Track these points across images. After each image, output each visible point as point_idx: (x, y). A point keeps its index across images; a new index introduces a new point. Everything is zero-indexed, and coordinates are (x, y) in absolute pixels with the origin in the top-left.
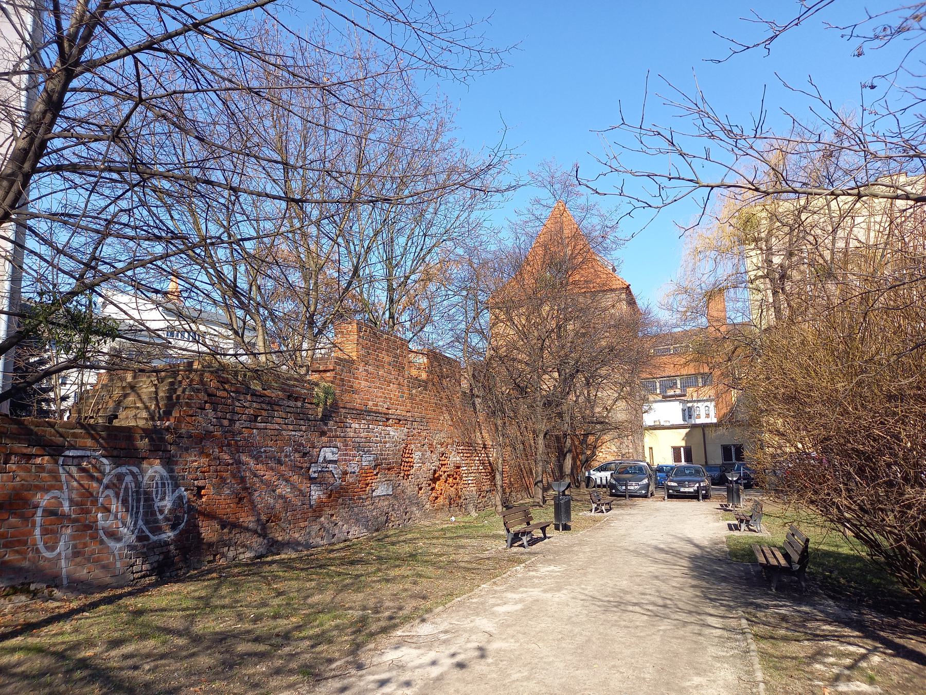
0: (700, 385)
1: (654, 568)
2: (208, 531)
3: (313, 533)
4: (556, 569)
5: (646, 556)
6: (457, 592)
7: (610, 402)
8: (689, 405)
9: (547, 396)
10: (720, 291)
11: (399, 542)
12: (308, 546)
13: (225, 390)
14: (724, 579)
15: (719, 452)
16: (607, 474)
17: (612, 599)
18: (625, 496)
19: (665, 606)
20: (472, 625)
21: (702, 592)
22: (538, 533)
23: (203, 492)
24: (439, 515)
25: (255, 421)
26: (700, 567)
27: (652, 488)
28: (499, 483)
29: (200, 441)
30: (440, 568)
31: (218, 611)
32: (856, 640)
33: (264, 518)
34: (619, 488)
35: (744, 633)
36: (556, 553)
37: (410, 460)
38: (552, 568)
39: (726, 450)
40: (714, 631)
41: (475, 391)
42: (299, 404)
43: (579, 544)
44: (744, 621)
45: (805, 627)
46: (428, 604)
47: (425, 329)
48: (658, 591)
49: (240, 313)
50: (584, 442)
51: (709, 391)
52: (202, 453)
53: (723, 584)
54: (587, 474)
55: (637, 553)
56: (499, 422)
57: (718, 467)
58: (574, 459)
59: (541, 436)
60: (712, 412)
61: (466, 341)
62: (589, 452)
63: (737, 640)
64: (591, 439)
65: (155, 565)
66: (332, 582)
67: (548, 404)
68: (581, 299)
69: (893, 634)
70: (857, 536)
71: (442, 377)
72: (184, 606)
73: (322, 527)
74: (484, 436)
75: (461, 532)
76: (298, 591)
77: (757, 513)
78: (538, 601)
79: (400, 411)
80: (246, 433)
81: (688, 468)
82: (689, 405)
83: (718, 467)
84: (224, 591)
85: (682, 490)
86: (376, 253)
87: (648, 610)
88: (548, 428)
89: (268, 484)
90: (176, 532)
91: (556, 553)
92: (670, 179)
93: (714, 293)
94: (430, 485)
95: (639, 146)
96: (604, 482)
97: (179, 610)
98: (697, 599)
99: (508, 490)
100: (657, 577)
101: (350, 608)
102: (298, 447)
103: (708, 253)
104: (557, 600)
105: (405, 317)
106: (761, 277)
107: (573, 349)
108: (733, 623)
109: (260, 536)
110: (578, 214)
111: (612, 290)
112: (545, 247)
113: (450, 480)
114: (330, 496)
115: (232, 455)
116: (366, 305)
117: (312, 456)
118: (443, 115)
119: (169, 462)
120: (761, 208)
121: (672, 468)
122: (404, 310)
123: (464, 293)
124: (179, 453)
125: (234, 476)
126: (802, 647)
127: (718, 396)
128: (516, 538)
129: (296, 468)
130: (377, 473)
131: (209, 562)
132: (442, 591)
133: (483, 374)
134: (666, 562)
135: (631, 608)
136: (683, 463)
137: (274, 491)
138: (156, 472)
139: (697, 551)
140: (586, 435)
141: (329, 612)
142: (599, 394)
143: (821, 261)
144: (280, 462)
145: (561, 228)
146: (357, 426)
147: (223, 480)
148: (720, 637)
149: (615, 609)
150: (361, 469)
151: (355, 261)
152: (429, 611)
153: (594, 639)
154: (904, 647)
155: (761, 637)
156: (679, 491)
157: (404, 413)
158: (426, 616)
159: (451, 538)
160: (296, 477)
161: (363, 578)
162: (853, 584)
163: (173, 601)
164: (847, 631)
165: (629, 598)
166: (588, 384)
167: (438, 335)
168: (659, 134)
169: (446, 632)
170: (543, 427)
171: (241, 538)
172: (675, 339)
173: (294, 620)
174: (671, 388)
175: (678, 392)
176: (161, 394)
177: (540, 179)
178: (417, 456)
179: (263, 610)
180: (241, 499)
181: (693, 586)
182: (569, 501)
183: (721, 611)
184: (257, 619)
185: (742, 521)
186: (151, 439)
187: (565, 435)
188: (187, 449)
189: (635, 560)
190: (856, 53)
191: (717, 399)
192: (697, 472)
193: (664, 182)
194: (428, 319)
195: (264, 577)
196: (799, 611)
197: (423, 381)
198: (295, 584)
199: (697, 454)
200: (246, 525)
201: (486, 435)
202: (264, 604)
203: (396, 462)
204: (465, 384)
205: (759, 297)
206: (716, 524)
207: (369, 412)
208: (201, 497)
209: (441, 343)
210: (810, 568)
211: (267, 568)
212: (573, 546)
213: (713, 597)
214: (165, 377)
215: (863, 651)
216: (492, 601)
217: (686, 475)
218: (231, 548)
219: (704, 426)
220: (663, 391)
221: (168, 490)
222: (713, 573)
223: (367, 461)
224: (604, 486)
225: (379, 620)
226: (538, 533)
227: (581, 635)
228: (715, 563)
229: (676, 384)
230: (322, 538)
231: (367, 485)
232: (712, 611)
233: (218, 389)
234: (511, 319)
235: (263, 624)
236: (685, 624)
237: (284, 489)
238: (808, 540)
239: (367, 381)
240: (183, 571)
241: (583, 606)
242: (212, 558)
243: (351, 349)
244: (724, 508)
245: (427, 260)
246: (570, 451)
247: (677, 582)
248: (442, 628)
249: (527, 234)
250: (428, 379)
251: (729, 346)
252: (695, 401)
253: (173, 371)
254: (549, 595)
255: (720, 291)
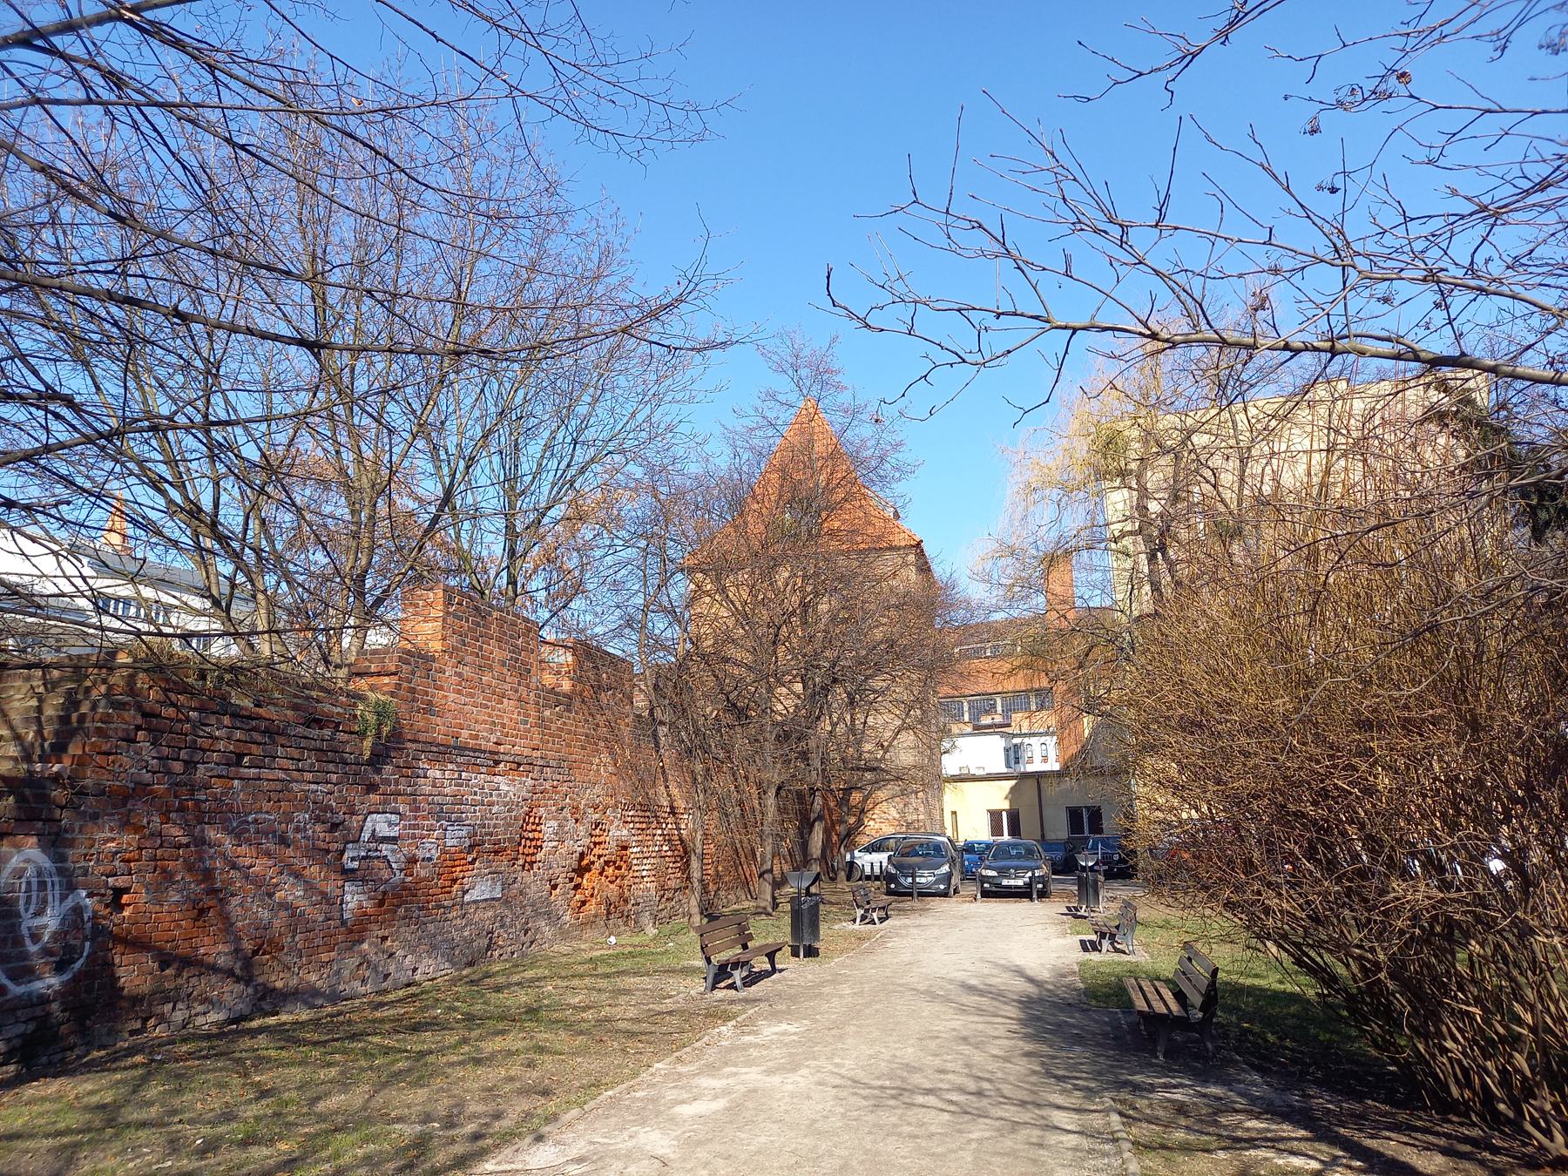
0: (1033, 708)
1: (959, 1023)
2: (133, 974)
3: (346, 973)
4: (791, 1029)
5: (947, 1000)
6: (608, 1079)
7: (888, 734)
8: (1017, 741)
9: (782, 724)
10: (1068, 553)
11: (509, 985)
12: (335, 997)
13: (173, 705)
14: (1078, 1040)
15: (1063, 818)
16: (881, 858)
17: (887, 1083)
18: (910, 895)
19: (979, 1093)
20: (630, 1144)
21: (1043, 1064)
22: (761, 964)
23: (125, 898)
24: (588, 934)
25: (239, 764)
26: (1039, 1019)
27: (955, 880)
28: (696, 875)
29: (122, 802)
30: (581, 1033)
31: (130, 1134)
32: (1303, 1146)
33: (247, 946)
34: (902, 880)
35: (1117, 1140)
36: (793, 999)
37: (536, 835)
38: (784, 1027)
39: (1074, 815)
40: (1065, 1138)
41: (658, 713)
42: (327, 732)
43: (833, 982)
44: (1115, 1118)
45: (1216, 1123)
46: (552, 1106)
47: (572, 605)
48: (967, 1065)
49: (226, 568)
50: (844, 801)
51: (1048, 719)
52: (126, 824)
53: (1078, 1049)
54: (848, 857)
55: (932, 996)
56: (699, 767)
57: (1064, 843)
58: (827, 832)
59: (772, 793)
60: (1052, 753)
61: (644, 627)
62: (852, 820)
63: (1105, 1154)
64: (856, 797)
65: (17, 1042)
66: (371, 1068)
67: (784, 737)
68: (841, 561)
69: (1360, 1130)
70: (1299, 962)
71: (598, 688)
72: (61, 1126)
73: (365, 961)
74: (673, 792)
75: (626, 965)
76: (299, 1088)
77: (1129, 920)
78: (755, 1091)
79: (521, 749)
80: (218, 787)
81: (1014, 846)
82: (1017, 741)
83: (1064, 843)
84: (153, 1090)
85: (1005, 882)
86: (487, 471)
87: (951, 1102)
88: (784, 777)
89: (259, 882)
90: (66, 977)
91: (793, 999)
92: (998, 315)
93: (1053, 560)
94: (571, 880)
95: (945, 242)
96: (877, 870)
97: (47, 1136)
98: (1034, 1079)
99: (712, 887)
100: (965, 1039)
101: (399, 1120)
102: (321, 813)
103: (1047, 492)
104: (790, 1087)
105: (537, 583)
106: (1131, 533)
107: (828, 642)
108: (1097, 1121)
109: (238, 980)
110: (839, 419)
111: (891, 548)
112: (783, 471)
113: (610, 871)
114: (381, 903)
115: (187, 827)
116: (464, 557)
117: (349, 829)
118: (611, 237)
119: (55, 842)
120: (1129, 423)
121: (989, 846)
122: (535, 571)
123: (642, 544)
124: (77, 825)
125: (190, 868)
126: (1216, 1162)
127: (1062, 726)
128: (722, 972)
129: (317, 852)
130: (474, 860)
131: (133, 1033)
132: (579, 1078)
133: (673, 685)
134: (980, 1011)
135: (920, 1099)
136: (1006, 837)
137: (271, 895)
138: (28, 861)
139: (1031, 989)
140: (848, 791)
141: (355, 1130)
142: (870, 720)
143: (1222, 509)
144: (283, 841)
145: (811, 441)
146: (438, 774)
147: (168, 876)
148: (1075, 1149)
149: (892, 1102)
150: (444, 852)
151: (447, 480)
152: (552, 1118)
153: (854, 1163)
154: (1380, 1155)
155: (1146, 1147)
156: (999, 885)
157: (527, 752)
158: (545, 1129)
159: (607, 976)
160: (315, 869)
161: (431, 1059)
162: (1288, 1043)
163: (41, 1115)
164: (1286, 1130)
165: (917, 1079)
166: (852, 702)
167: (594, 614)
168: (980, 226)
169: (580, 1160)
170: (775, 776)
171: (200, 985)
172: (996, 631)
173: (283, 1146)
174: (987, 712)
175: (998, 719)
176: (49, 712)
177: (775, 358)
178: (549, 827)
179: (222, 1129)
180: (202, 912)
181: (1028, 1054)
182: (817, 905)
183: (1075, 1099)
184: (211, 1146)
185: (1103, 936)
186: (21, 799)
187: (813, 791)
188: (95, 817)
189: (928, 1009)
190: (1308, 128)
191: (1062, 730)
192: (1030, 852)
193: (990, 319)
194: (578, 589)
195: (238, 1061)
196: (1204, 1096)
197: (565, 695)
198: (296, 1073)
199: (1028, 823)
200: (211, 960)
201: (675, 791)
202: (228, 1116)
203: (511, 840)
204: (640, 701)
205: (1129, 564)
206: (1062, 941)
207: (462, 749)
208: (121, 908)
209: (599, 630)
210: (1221, 1016)
211: (247, 1042)
212: (822, 984)
213: (1060, 1073)
214: (61, 679)
215: (1315, 1165)
216: (671, 1095)
217: (1011, 857)
218: (180, 1005)
219: (1039, 776)
220: (975, 717)
221: (53, 894)
222: (1060, 1028)
223: (455, 838)
224: (877, 878)
225: (453, 1141)
226: (761, 964)
227: (831, 1155)
228: (1062, 1010)
229: (994, 706)
230: (364, 981)
231: (454, 881)
232: (1059, 1099)
233: (162, 703)
234: (723, 590)
235: (219, 1159)
236: (1015, 1126)
237: (290, 892)
238: (1215, 971)
239: (459, 692)
240: (77, 1051)
241: (836, 1098)
242: (138, 1025)
243: (428, 632)
244: (1073, 913)
245: (577, 485)
246: (820, 818)
247: (1000, 1048)
248: (574, 1152)
249: (752, 449)
250: (573, 692)
251: (1079, 645)
252: (1025, 735)
253: (77, 668)
254: (776, 1079)
255: (1068, 553)
